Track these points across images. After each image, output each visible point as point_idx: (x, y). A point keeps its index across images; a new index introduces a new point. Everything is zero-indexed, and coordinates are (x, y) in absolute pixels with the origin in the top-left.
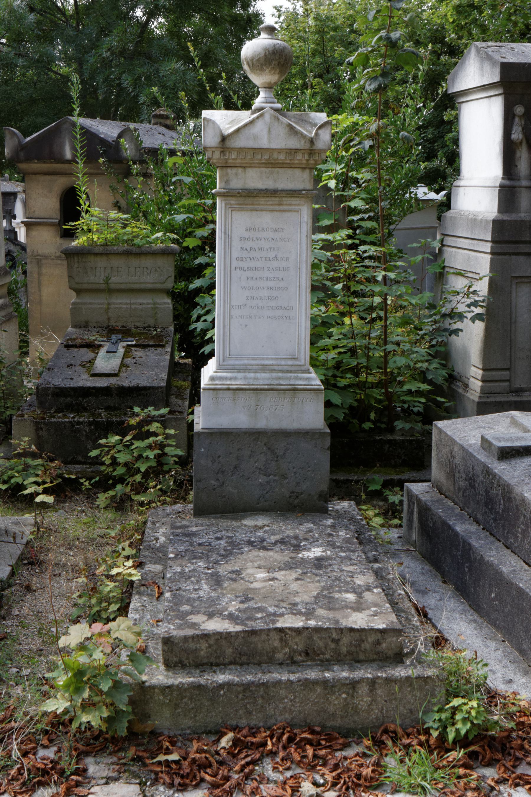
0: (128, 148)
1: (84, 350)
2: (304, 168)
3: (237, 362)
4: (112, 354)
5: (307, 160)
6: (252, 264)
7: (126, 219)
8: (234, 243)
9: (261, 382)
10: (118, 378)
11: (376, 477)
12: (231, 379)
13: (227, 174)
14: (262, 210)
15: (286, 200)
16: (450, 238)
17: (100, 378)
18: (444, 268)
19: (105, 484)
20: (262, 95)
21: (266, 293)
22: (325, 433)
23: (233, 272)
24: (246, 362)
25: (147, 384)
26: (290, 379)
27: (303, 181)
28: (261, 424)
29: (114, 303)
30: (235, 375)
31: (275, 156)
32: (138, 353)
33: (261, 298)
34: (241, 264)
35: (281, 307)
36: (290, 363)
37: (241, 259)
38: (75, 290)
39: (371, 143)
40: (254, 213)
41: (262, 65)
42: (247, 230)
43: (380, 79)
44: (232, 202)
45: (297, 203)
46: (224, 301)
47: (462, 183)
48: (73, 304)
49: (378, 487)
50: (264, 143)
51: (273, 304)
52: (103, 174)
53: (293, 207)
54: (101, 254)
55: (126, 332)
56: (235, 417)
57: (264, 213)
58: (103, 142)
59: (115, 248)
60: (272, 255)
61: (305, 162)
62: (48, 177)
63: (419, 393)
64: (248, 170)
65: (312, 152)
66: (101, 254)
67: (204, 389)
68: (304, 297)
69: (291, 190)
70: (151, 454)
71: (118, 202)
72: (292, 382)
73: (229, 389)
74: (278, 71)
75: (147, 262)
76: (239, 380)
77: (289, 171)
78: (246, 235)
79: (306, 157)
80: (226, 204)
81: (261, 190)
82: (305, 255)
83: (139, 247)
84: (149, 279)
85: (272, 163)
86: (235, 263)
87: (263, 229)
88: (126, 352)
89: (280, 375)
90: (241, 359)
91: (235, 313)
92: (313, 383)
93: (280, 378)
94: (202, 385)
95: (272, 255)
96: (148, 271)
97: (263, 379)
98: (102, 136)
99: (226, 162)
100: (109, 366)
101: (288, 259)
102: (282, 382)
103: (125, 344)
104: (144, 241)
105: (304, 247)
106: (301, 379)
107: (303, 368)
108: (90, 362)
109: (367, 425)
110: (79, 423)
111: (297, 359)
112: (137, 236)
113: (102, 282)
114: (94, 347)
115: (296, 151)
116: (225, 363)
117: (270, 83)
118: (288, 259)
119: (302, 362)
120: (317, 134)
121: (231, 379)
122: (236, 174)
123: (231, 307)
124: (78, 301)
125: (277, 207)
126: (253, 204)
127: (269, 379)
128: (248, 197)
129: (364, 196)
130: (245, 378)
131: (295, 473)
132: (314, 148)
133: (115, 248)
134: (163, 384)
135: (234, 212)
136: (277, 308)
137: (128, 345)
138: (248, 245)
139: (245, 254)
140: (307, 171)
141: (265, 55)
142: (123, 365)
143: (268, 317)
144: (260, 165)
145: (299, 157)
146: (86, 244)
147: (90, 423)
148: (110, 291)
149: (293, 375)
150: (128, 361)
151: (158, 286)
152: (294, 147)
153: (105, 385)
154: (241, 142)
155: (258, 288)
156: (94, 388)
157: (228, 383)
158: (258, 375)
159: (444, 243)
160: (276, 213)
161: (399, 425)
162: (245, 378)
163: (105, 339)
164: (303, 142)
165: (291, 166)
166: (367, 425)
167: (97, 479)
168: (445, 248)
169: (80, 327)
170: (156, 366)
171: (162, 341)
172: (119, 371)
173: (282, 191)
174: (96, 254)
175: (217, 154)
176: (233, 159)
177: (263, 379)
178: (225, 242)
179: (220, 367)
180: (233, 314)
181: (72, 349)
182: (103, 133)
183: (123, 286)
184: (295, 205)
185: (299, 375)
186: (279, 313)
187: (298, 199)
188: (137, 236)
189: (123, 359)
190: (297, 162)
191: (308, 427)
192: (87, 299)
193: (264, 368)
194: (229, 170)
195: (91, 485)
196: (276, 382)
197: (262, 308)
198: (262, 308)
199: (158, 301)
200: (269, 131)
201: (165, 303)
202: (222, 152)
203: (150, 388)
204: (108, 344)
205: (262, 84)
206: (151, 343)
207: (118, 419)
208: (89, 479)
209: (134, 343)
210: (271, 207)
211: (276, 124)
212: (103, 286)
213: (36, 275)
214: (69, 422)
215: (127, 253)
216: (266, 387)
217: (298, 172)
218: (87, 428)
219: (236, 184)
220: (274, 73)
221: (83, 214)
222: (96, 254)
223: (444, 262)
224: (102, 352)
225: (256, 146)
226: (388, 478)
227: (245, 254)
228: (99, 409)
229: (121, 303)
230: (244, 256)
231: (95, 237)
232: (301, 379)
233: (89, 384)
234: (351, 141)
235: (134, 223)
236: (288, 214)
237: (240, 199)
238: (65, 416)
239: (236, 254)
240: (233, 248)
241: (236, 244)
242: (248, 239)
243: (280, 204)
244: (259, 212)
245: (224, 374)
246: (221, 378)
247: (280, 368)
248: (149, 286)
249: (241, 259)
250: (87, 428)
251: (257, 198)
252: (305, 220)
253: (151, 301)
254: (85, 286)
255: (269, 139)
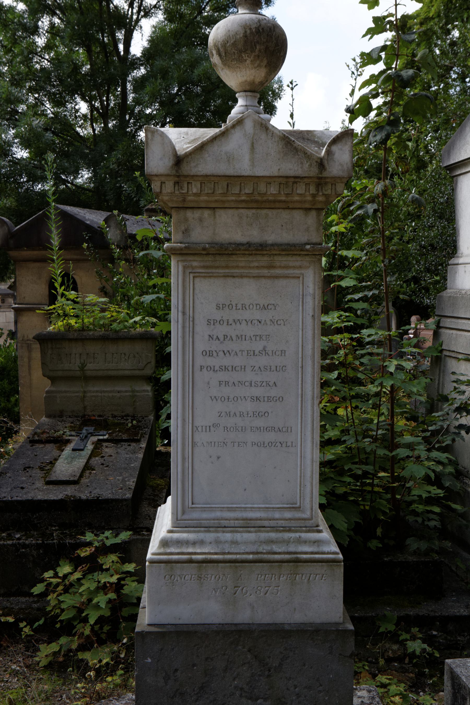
0: (112, 235)
1: (49, 447)
2: (307, 210)
3: (205, 515)
4: (77, 453)
5: (314, 196)
6: (227, 361)
7: (103, 303)
8: (197, 329)
9: (242, 548)
10: (77, 487)
11: (388, 611)
12: (194, 543)
13: (186, 220)
14: (242, 277)
15: (280, 260)
16: (449, 320)
17: (56, 487)
18: (441, 351)
19: (52, 629)
20: (241, 102)
21: (249, 406)
22: (346, 631)
23: (198, 374)
24: (218, 514)
25: (110, 496)
26: (287, 542)
27: (307, 230)
28: (244, 616)
29: (90, 391)
30: (201, 536)
31: (262, 188)
32: (108, 450)
33: (242, 415)
34: (210, 361)
35: (273, 429)
36: (288, 515)
37: (210, 354)
38: (49, 378)
39: (375, 206)
40: (230, 281)
41: (240, 52)
42: (218, 307)
43: (388, 128)
44: (195, 264)
45: (298, 264)
46: (184, 420)
47: (461, 261)
48: (47, 392)
49: (392, 627)
50: (244, 167)
51: (259, 422)
52: (87, 260)
53: (291, 271)
54: (76, 340)
55: (101, 424)
56: (203, 606)
57: (245, 280)
58: (89, 228)
59: (91, 333)
60: (258, 346)
61: (309, 198)
62: (38, 264)
63: (430, 501)
64: (220, 212)
65: (321, 182)
66: (76, 340)
67: (152, 562)
68: (309, 413)
69: (288, 244)
70: (101, 600)
71: (104, 287)
72: (292, 548)
73: (190, 561)
74: (265, 62)
75: (125, 348)
76: (206, 547)
77: (285, 214)
78: (217, 315)
79: (312, 190)
80: (185, 268)
81: (242, 244)
82: (310, 346)
83: (116, 332)
84: (126, 366)
85: (257, 201)
86: (200, 361)
87: (244, 307)
88: (95, 448)
89: (273, 535)
90: (211, 509)
91: (201, 437)
92: (326, 549)
93: (272, 542)
94: (149, 556)
95: (258, 346)
96: (126, 358)
97: (245, 543)
98: (88, 222)
99: (184, 200)
100: (70, 470)
101: (283, 352)
102: (276, 548)
103: (95, 439)
104: (121, 326)
105: (309, 334)
106: (305, 542)
107: (309, 523)
108: (51, 463)
109: (374, 544)
110: (24, 546)
111: (298, 509)
112: (115, 321)
113: (78, 369)
114: (61, 443)
115: (297, 179)
116: (186, 517)
117: (252, 83)
118: (283, 352)
119: (307, 515)
120: (329, 152)
121: (194, 543)
122: (201, 220)
123: (194, 429)
124: (53, 389)
125: (265, 272)
126: (227, 267)
127: (254, 543)
128: (219, 256)
129: (354, 276)
130: (218, 542)
131: (298, 695)
132: (325, 174)
133: (91, 333)
134: (129, 495)
135: (197, 280)
136: (267, 429)
137: (99, 440)
138: (220, 331)
139: (215, 346)
140: (314, 213)
141: (245, 36)
142: (87, 467)
143: (253, 444)
144: (239, 205)
145: (301, 189)
146: (62, 329)
147: (38, 547)
148: (87, 378)
149: (293, 535)
150: (96, 461)
151: (137, 373)
152: (292, 173)
153: (60, 497)
154: (207, 166)
155: (236, 399)
156: (46, 501)
157: (190, 550)
158: (238, 536)
159: (441, 325)
160: (264, 281)
161: (413, 544)
162: (218, 542)
163: (73, 433)
164: (306, 165)
165: (287, 206)
166: (374, 544)
167: (41, 622)
168: (443, 331)
169: (55, 417)
170: (125, 468)
171: (136, 434)
172: (81, 476)
173: (272, 245)
174: (70, 340)
175: (169, 187)
176: (195, 195)
177: (246, 543)
178: (184, 327)
179: (178, 523)
180: (197, 439)
181: (37, 445)
182: (89, 220)
183: (100, 373)
184: (294, 267)
185: (303, 535)
186: (271, 436)
187: (299, 258)
188: (115, 321)
189: (90, 458)
190: (297, 198)
191: (318, 621)
192: (63, 387)
193: (248, 525)
194: (189, 214)
195: (33, 630)
196: (267, 548)
197: (243, 429)
198: (243, 429)
199: (137, 389)
200: (252, 148)
201: (144, 391)
202: (176, 183)
203: (112, 500)
204: (76, 438)
205: (242, 84)
206: (125, 437)
207: (72, 541)
208: (30, 623)
209: (105, 437)
210: (256, 272)
211: (263, 136)
212: (78, 373)
213: (26, 360)
214: (13, 545)
215: (104, 339)
216: (251, 556)
217: (298, 215)
218: (34, 553)
219: (201, 235)
220: (259, 66)
221: (59, 298)
222: (70, 340)
223: (441, 346)
224: (68, 450)
225: (231, 172)
226: (403, 613)
227: (215, 346)
228: (52, 526)
229: (97, 391)
230: (214, 348)
231: (72, 322)
232: (305, 542)
233: (40, 496)
234: (350, 205)
235: (113, 307)
236: (283, 282)
237: (206, 258)
238: (10, 537)
239: (201, 346)
240: (197, 337)
241: (202, 330)
242: (221, 322)
243: (271, 267)
244: (237, 280)
245: (184, 536)
246: (179, 543)
247: (272, 523)
248: (127, 373)
249: (210, 354)
250: (34, 553)
251: (234, 257)
252: (311, 290)
253: (130, 389)
254: (60, 374)
255: (252, 160)
